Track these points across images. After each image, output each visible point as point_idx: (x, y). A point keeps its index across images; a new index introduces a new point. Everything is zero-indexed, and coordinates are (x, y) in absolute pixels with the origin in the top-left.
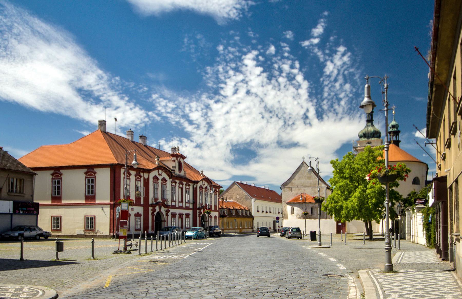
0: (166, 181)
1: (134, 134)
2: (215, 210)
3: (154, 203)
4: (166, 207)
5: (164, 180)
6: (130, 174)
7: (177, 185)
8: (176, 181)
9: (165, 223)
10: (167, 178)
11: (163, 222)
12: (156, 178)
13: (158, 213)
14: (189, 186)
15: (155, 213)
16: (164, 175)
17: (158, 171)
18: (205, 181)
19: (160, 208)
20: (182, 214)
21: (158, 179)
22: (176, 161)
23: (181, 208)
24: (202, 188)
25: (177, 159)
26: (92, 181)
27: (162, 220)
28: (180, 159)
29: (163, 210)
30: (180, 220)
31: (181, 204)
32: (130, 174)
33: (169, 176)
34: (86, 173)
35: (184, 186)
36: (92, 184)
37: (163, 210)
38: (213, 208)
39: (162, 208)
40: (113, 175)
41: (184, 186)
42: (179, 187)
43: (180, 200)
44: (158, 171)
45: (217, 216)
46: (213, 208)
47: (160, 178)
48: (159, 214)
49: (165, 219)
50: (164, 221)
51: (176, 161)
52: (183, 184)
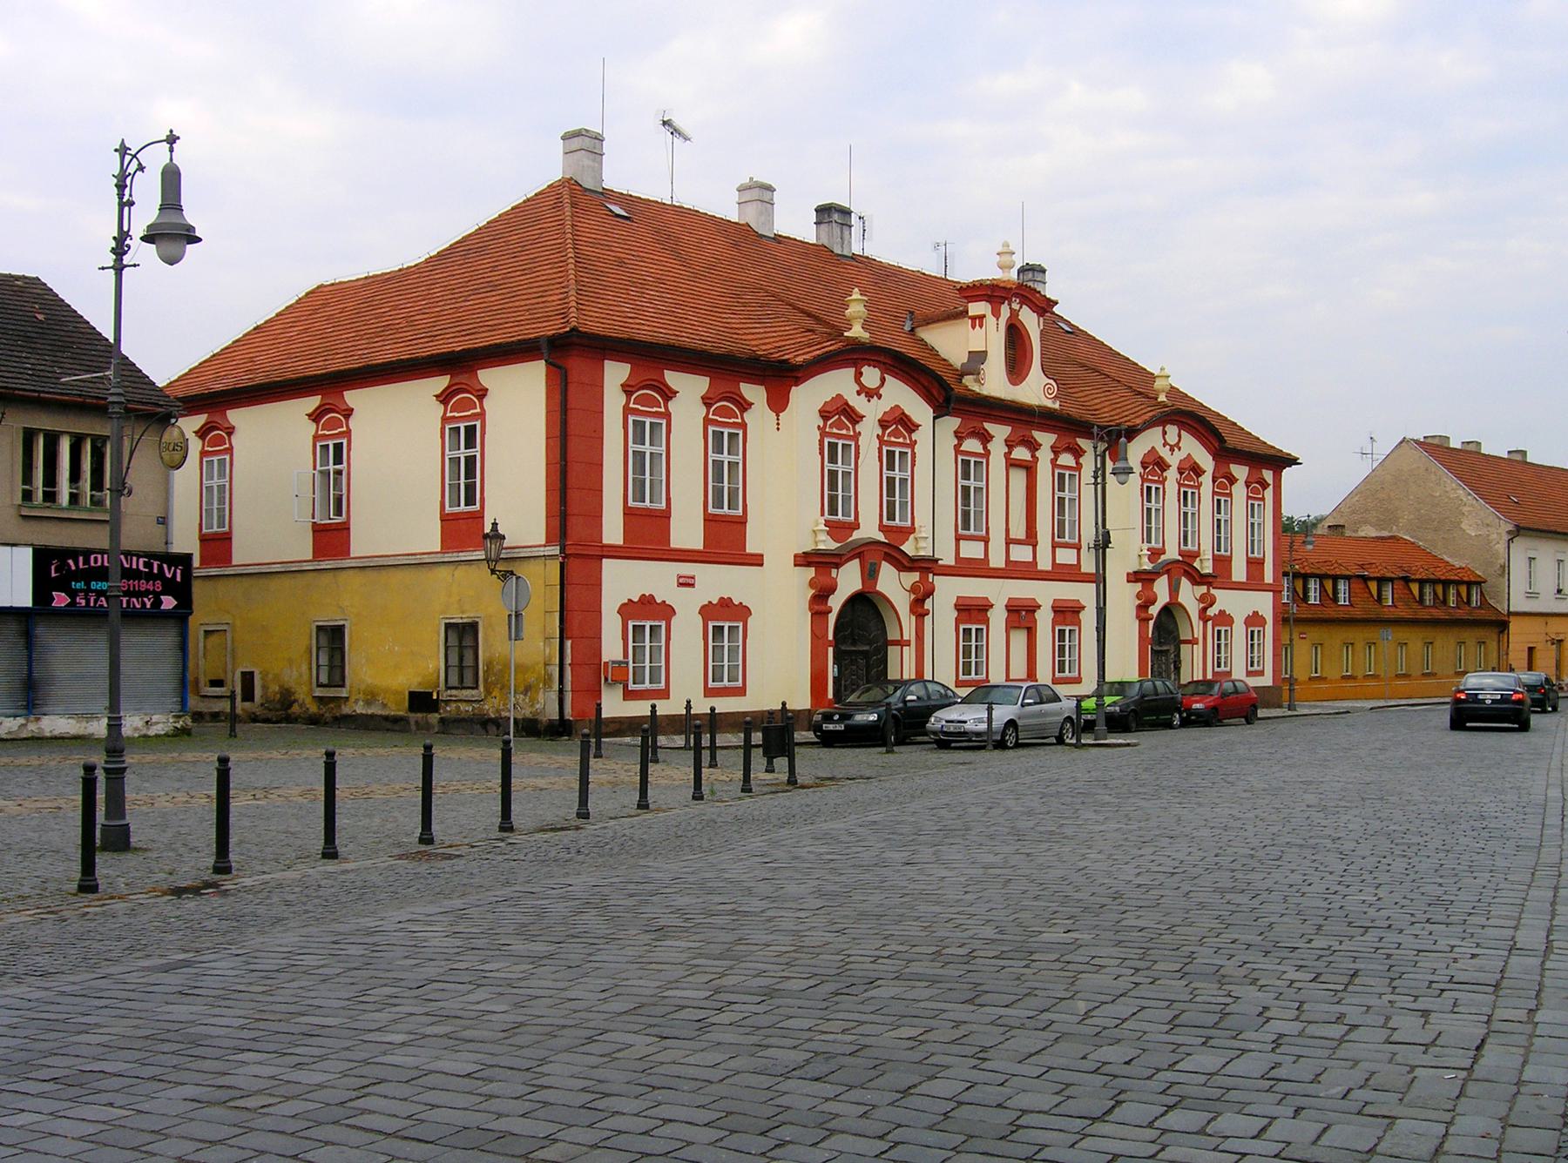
0: (910, 426)
1: (777, 197)
2: (1254, 582)
3: (1148, 566)
4: (911, 569)
5: (1191, 470)
6: (1232, 480)
7: (997, 448)
8: (990, 427)
9: (909, 653)
10: (919, 410)
11: (893, 652)
12: (1155, 464)
13: (1166, 610)
14: (1078, 453)
15: (1154, 610)
16: (900, 395)
17: (859, 375)
18: (1182, 426)
19: (1174, 590)
20: (1031, 608)
21: (855, 417)
22: (990, 320)
23: (1027, 571)
24: (1162, 465)
25: (996, 314)
26: (471, 431)
27: (892, 635)
28: (1014, 314)
29: (893, 585)
30: (1019, 638)
31: (1021, 554)
32: (1232, 480)
33: (929, 398)
34: (444, 398)
35: (1045, 455)
36: (470, 452)
37: (1189, 595)
38: (1239, 573)
39: (1185, 583)
40: (558, 398)
41: (1045, 455)
42: (1012, 464)
43: (1019, 531)
44: (859, 375)
45: (1267, 612)
46: (1239, 573)
47: (1174, 460)
48: (865, 604)
49: (1198, 633)
50: (902, 643)
51: (990, 320)
52: (1078, 453)
